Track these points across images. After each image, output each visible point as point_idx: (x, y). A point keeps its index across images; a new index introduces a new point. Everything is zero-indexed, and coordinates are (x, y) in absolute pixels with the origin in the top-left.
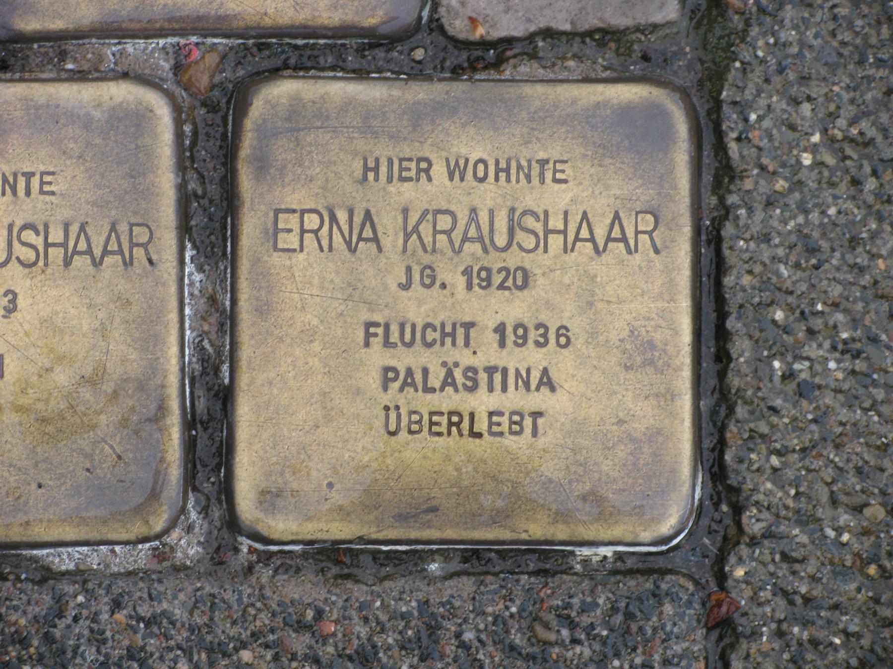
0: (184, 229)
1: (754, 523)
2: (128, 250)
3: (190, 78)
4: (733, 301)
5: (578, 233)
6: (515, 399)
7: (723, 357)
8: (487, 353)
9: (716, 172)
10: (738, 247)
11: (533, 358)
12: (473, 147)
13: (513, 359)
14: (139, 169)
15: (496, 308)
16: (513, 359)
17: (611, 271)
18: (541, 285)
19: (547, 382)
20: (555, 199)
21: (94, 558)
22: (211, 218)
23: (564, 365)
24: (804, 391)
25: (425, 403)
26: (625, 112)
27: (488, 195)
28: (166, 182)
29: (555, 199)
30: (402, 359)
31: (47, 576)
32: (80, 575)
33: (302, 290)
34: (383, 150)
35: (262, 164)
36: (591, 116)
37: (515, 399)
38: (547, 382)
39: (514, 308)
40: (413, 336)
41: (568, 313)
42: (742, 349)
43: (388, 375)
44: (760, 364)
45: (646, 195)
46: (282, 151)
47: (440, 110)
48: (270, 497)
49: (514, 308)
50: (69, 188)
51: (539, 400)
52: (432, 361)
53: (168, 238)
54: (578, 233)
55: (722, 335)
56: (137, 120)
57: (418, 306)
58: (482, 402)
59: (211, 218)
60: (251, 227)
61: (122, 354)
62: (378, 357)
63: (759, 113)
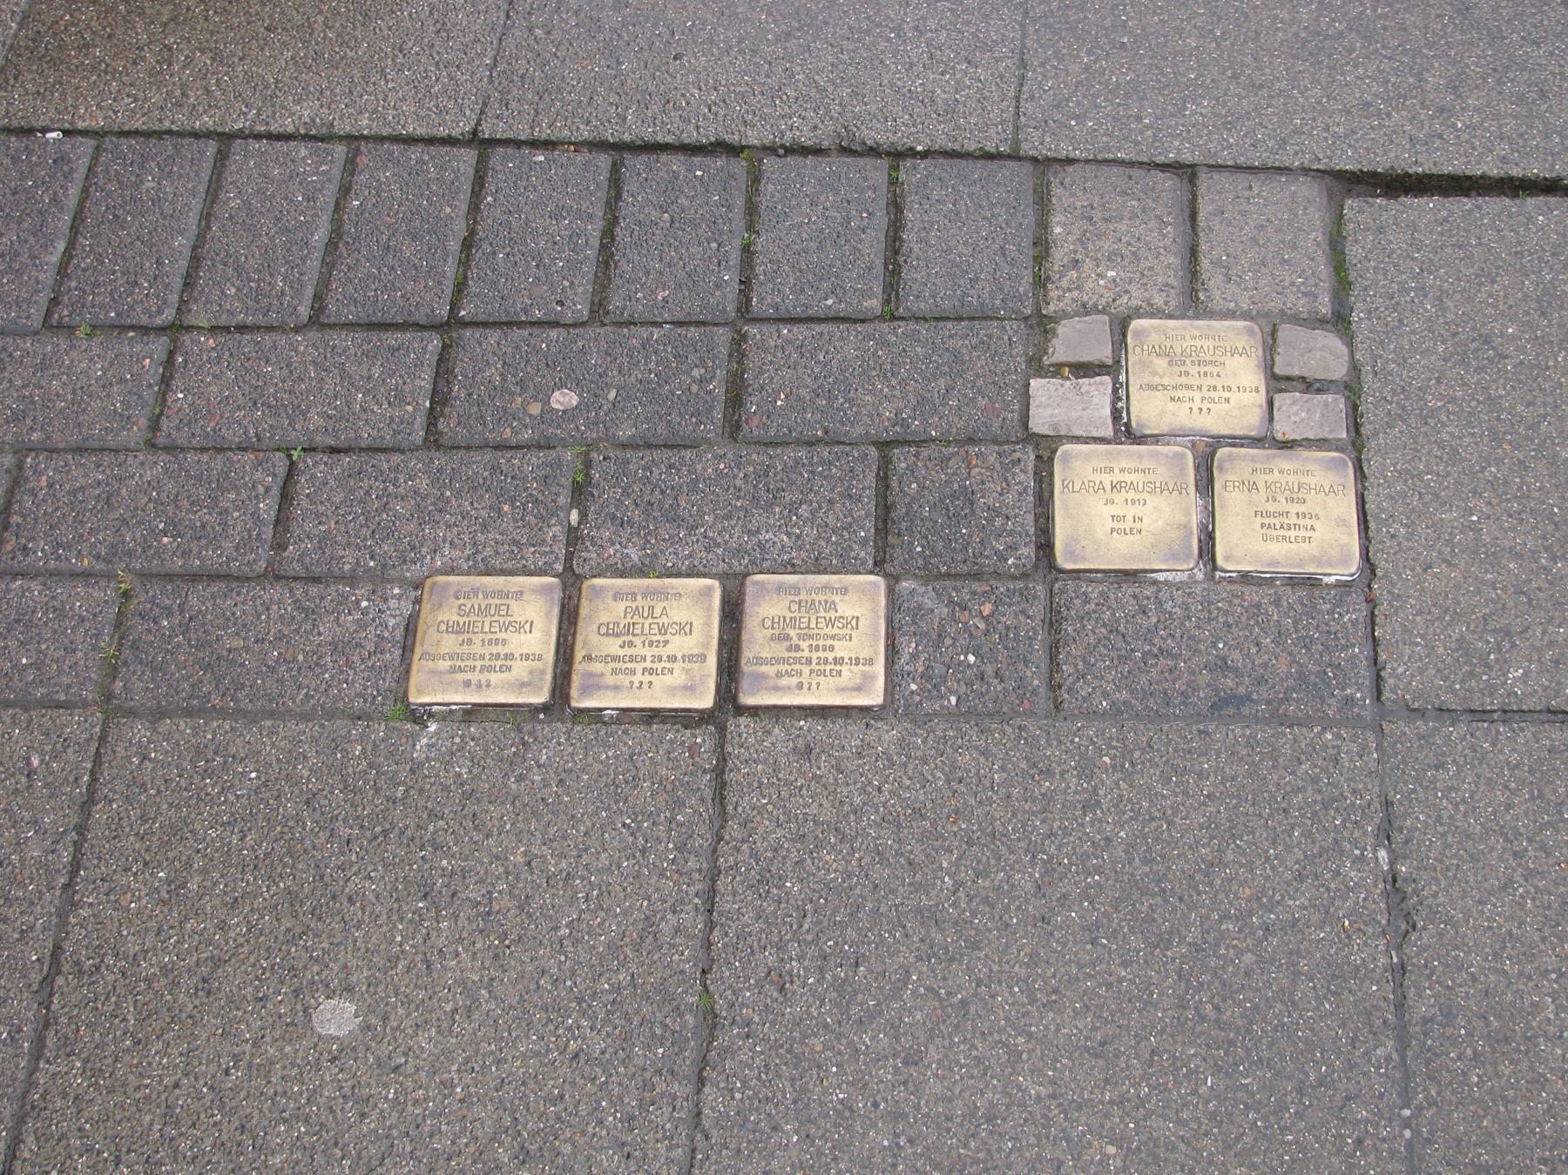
0: (1197, 490)
1: (1379, 573)
2: (1180, 490)
3: (1174, 557)
4: (1369, 513)
5: (1320, 489)
6: (1302, 533)
7: (1367, 528)
8: (1293, 520)
9: (1360, 474)
10: (1369, 498)
11: (1309, 522)
12: (1286, 466)
13: (1301, 522)
14: (1183, 470)
15: (1294, 508)
16: (1301, 522)
17: (1331, 500)
18: (1309, 503)
19: (1312, 528)
20: (1313, 480)
21: (1170, 576)
22: (1206, 484)
23: (1317, 525)
24: (1393, 536)
25: (1275, 533)
26: (1333, 459)
27: (1291, 479)
28: (1191, 472)
29: (1313, 480)
30: (1267, 521)
31: (1155, 582)
32: (1166, 582)
33: (1234, 505)
34: (1258, 466)
35: (1221, 469)
36: (1322, 460)
37: (1302, 533)
38: (1312, 528)
39: (1302, 509)
40: (1269, 514)
41: (1318, 510)
42: (1372, 525)
43: (1263, 525)
44: (1379, 530)
45: (1341, 481)
46: (1227, 465)
47: (1275, 456)
48: (1227, 559)
49: (1302, 509)
50: (1162, 473)
51: (1310, 533)
52: (1277, 522)
53: (1192, 489)
54: (1320, 489)
55: (1366, 521)
56: (1183, 456)
57: (1271, 507)
58: (1293, 533)
59: (1206, 484)
60: (1217, 485)
61: (1180, 518)
62: (1259, 520)
63: (1372, 466)
